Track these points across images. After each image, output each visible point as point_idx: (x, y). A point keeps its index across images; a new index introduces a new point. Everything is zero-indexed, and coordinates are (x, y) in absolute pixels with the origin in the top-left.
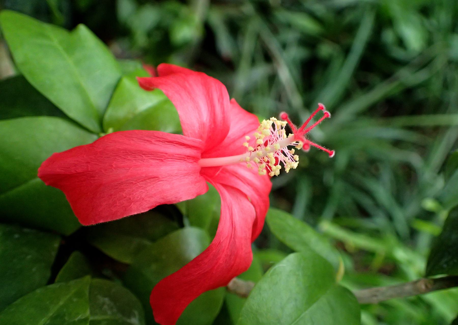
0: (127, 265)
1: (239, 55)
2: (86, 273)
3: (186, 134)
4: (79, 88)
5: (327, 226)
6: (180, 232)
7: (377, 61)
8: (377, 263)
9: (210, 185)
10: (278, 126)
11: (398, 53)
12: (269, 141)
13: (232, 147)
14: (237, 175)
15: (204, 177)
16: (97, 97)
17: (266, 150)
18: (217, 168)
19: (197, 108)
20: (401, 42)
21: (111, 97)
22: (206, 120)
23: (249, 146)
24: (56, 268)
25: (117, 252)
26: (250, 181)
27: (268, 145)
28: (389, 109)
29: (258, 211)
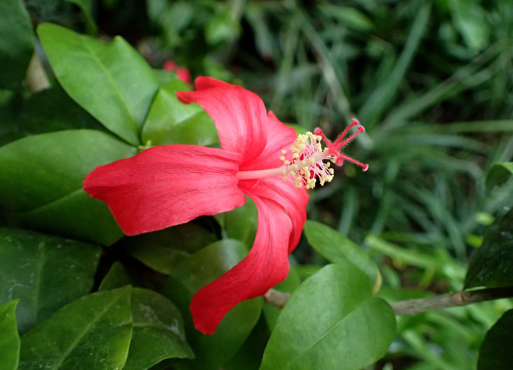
0: (166, 276)
1: (281, 54)
2: (126, 283)
3: (224, 148)
4: (117, 101)
5: (373, 241)
6: (218, 243)
7: (434, 60)
8: (427, 279)
9: (247, 197)
10: (313, 141)
11: (457, 51)
12: (304, 155)
13: (269, 160)
14: (274, 188)
15: (298, 45)
16: (135, 109)
17: (301, 163)
18: (254, 181)
19: (235, 122)
20: (460, 39)
21: (149, 109)
22: (244, 134)
23: (286, 160)
24: (98, 278)
25: (156, 263)
26: (288, 193)
27: (304, 159)
28: (446, 113)
29: (295, 223)
